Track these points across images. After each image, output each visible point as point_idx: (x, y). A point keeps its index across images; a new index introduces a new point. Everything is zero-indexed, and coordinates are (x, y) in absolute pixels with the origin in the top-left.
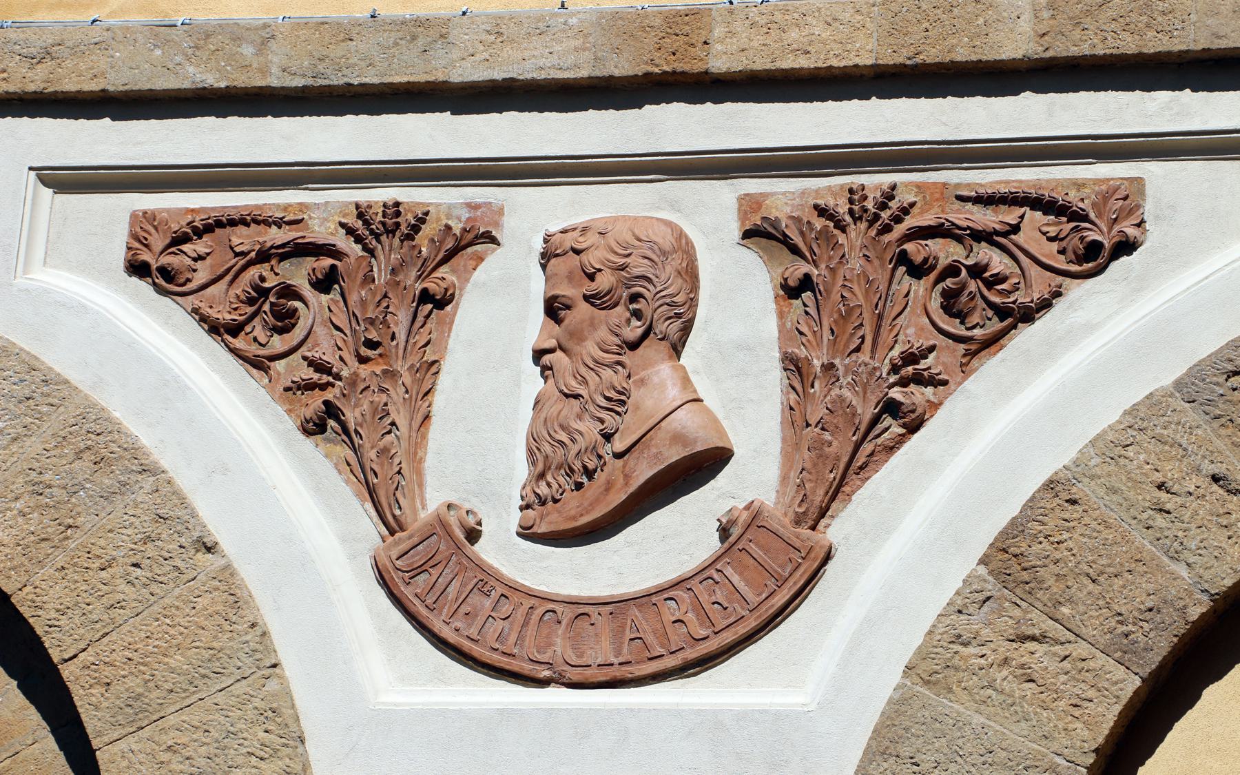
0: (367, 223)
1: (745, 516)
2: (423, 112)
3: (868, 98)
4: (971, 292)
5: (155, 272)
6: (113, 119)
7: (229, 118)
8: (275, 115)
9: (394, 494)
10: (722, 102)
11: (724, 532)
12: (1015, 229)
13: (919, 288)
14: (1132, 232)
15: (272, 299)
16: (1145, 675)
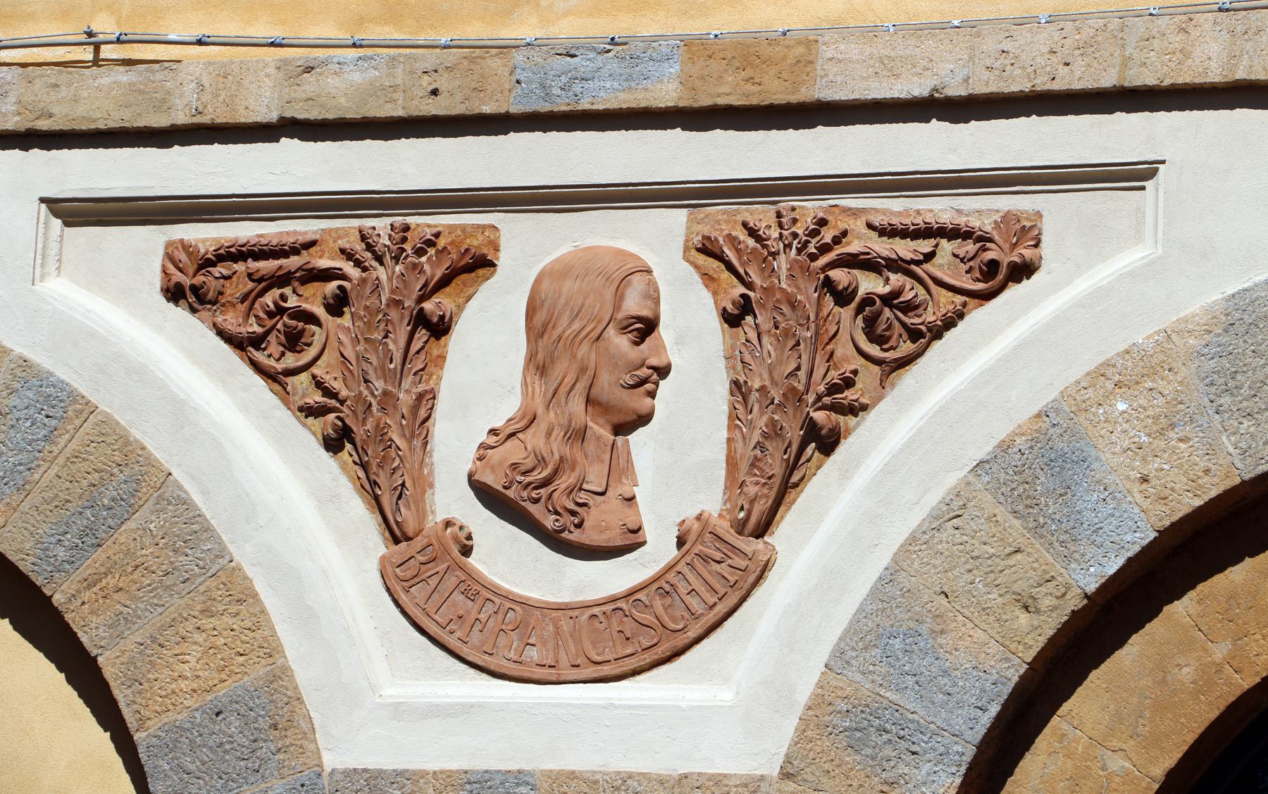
0: (369, 247)
1: (696, 526)
2: (604, 130)
3: (171, 146)
4: (888, 319)
5: (188, 293)
6: (683, 130)
7: (1195, 111)
8: (1040, 114)
9: (397, 504)
10: (61, 149)
11: (681, 542)
12: (929, 257)
13: (846, 313)
14: (1028, 253)
15: (285, 318)
16: (1029, 660)
